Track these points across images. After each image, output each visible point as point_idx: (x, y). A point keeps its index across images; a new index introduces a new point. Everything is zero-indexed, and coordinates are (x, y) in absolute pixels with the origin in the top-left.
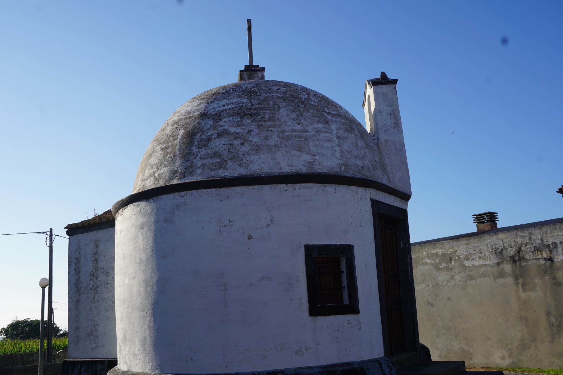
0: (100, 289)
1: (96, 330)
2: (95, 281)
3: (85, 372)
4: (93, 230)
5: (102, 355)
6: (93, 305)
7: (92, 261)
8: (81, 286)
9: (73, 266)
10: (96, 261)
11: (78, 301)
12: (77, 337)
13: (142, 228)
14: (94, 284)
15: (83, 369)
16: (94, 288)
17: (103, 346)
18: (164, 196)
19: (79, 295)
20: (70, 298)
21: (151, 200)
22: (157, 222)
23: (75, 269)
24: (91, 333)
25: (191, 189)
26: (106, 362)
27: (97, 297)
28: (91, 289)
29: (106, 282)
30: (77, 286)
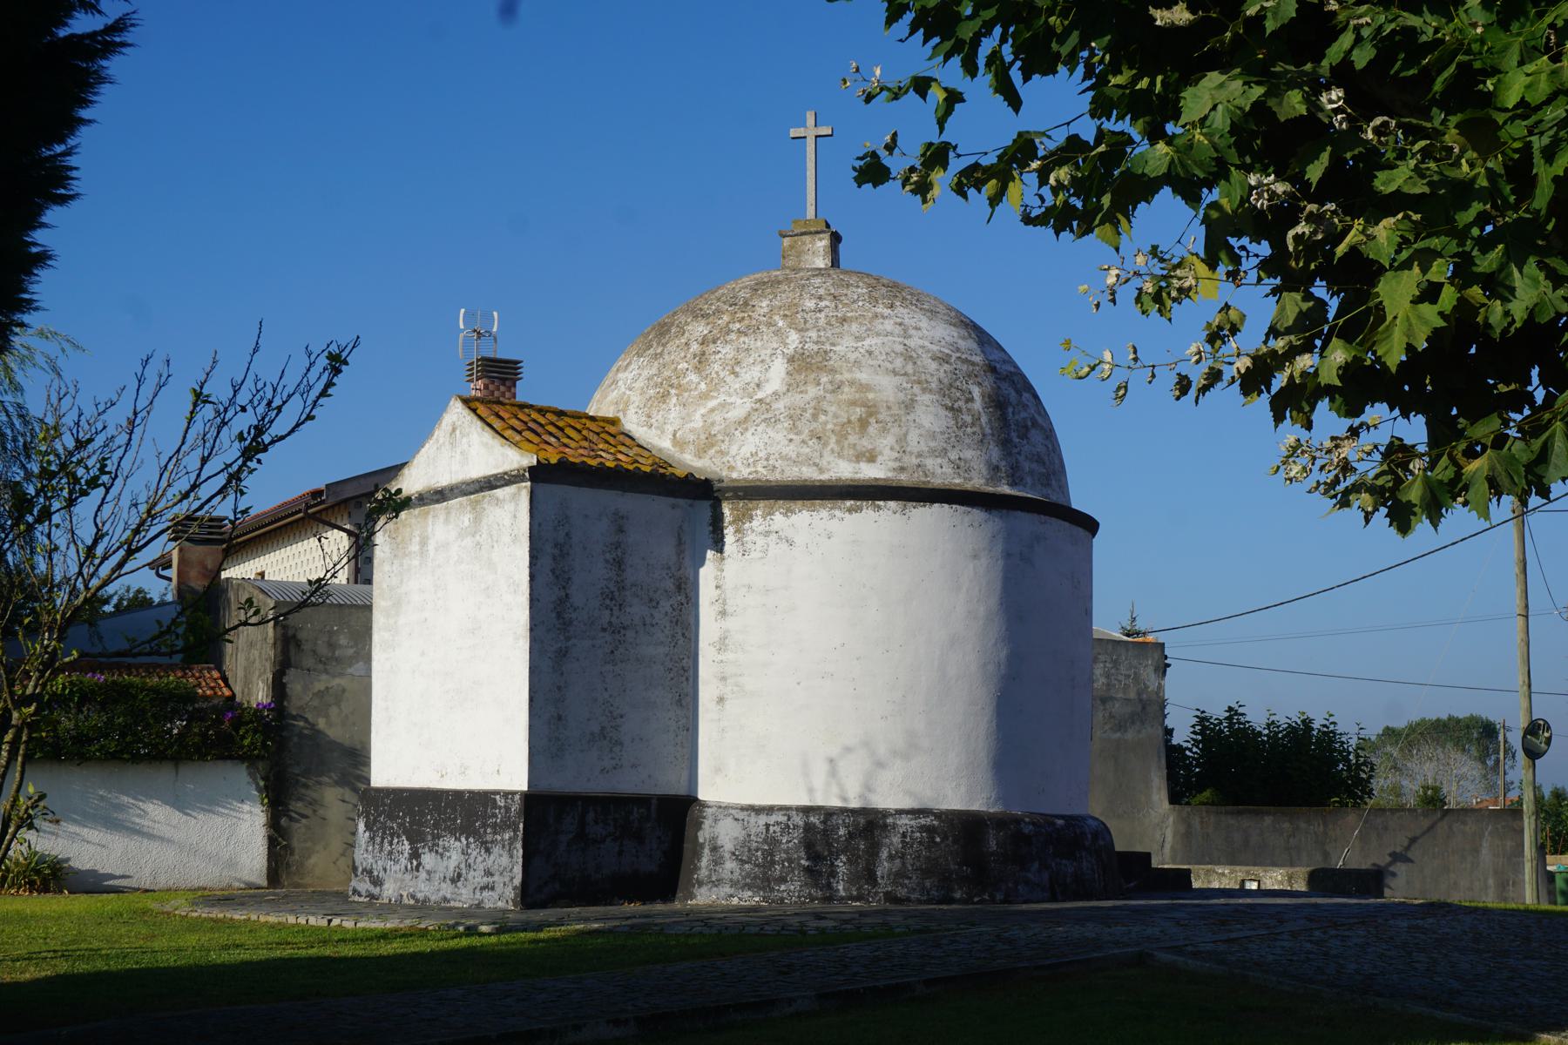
0: (630, 634)
1: (616, 728)
2: (616, 612)
3: (596, 822)
4: (611, 487)
5: (681, 790)
6: (609, 667)
7: (607, 561)
8: (574, 616)
9: (546, 562)
10: (619, 564)
11: (563, 654)
12: (558, 739)
13: (975, 557)
14: (614, 620)
15: (591, 816)
16: (616, 630)
17: (634, 766)
18: (1019, 513)
19: (568, 639)
20: (534, 640)
21: (995, 512)
22: (1008, 555)
23: (553, 571)
24: (603, 733)
25: (1051, 515)
26: (654, 802)
27: (621, 650)
28: (604, 630)
29: (648, 621)
30: (559, 615)
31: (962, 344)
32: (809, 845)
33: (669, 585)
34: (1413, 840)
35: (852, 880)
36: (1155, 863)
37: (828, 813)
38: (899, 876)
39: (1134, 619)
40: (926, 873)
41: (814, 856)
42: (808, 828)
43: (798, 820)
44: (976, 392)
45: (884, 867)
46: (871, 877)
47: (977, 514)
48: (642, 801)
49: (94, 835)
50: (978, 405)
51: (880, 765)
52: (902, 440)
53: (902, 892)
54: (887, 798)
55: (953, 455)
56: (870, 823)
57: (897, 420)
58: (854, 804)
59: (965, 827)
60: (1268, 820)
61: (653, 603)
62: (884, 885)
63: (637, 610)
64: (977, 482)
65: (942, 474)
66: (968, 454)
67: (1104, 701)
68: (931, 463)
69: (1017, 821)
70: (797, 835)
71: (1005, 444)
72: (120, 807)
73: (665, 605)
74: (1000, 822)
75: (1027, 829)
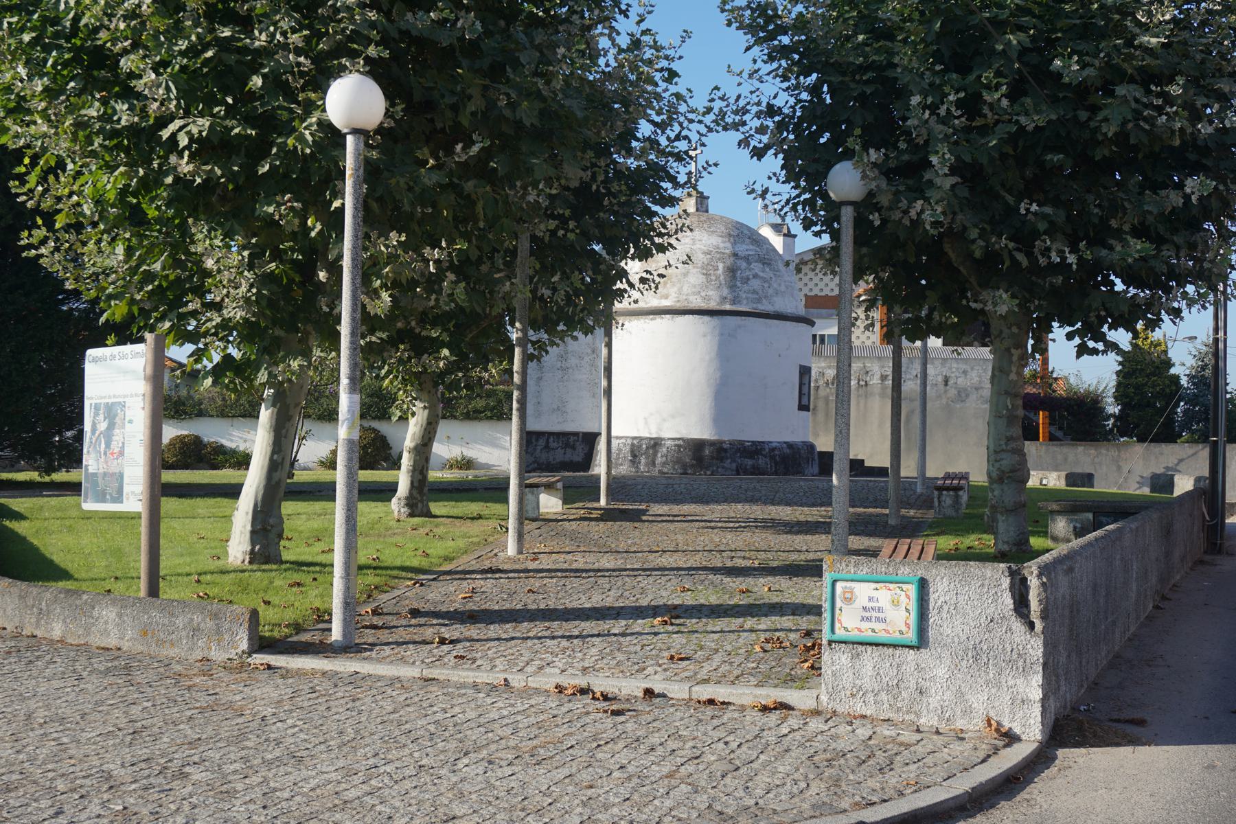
22: (722, 334)
24: (558, 409)
31: (722, 245)
32: (632, 451)
33: (589, 351)
34: (1181, 461)
35: (647, 464)
36: (866, 464)
37: (641, 439)
38: (664, 464)
39: (136, 395)
40: (675, 463)
41: (634, 456)
42: (633, 445)
43: (629, 442)
44: (721, 266)
45: (659, 460)
46: (654, 464)
47: (706, 318)
48: (576, 434)
49: (487, 449)
50: (720, 271)
51: (664, 420)
52: (680, 289)
53: (665, 470)
54: (666, 434)
55: (703, 294)
56: (656, 443)
57: (679, 281)
58: (654, 436)
59: (697, 446)
60: (1080, 449)
61: (581, 358)
62: (658, 467)
63: (573, 361)
64: (713, 305)
65: (696, 302)
66: (711, 293)
67: (977, 389)
68: (692, 298)
69: (721, 442)
70: (628, 447)
71: (732, 287)
72: (496, 438)
73: (587, 359)
74: (712, 443)
75: (725, 446)
